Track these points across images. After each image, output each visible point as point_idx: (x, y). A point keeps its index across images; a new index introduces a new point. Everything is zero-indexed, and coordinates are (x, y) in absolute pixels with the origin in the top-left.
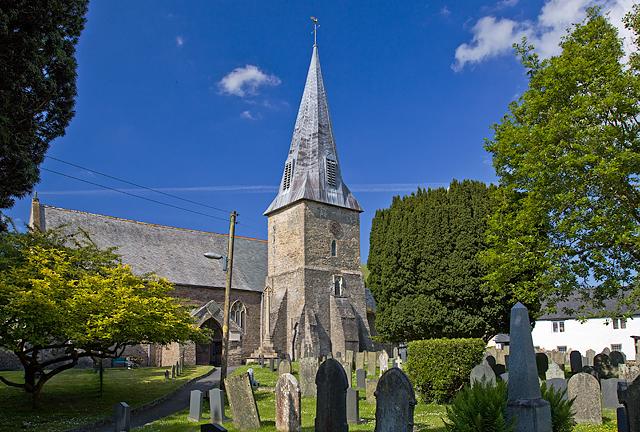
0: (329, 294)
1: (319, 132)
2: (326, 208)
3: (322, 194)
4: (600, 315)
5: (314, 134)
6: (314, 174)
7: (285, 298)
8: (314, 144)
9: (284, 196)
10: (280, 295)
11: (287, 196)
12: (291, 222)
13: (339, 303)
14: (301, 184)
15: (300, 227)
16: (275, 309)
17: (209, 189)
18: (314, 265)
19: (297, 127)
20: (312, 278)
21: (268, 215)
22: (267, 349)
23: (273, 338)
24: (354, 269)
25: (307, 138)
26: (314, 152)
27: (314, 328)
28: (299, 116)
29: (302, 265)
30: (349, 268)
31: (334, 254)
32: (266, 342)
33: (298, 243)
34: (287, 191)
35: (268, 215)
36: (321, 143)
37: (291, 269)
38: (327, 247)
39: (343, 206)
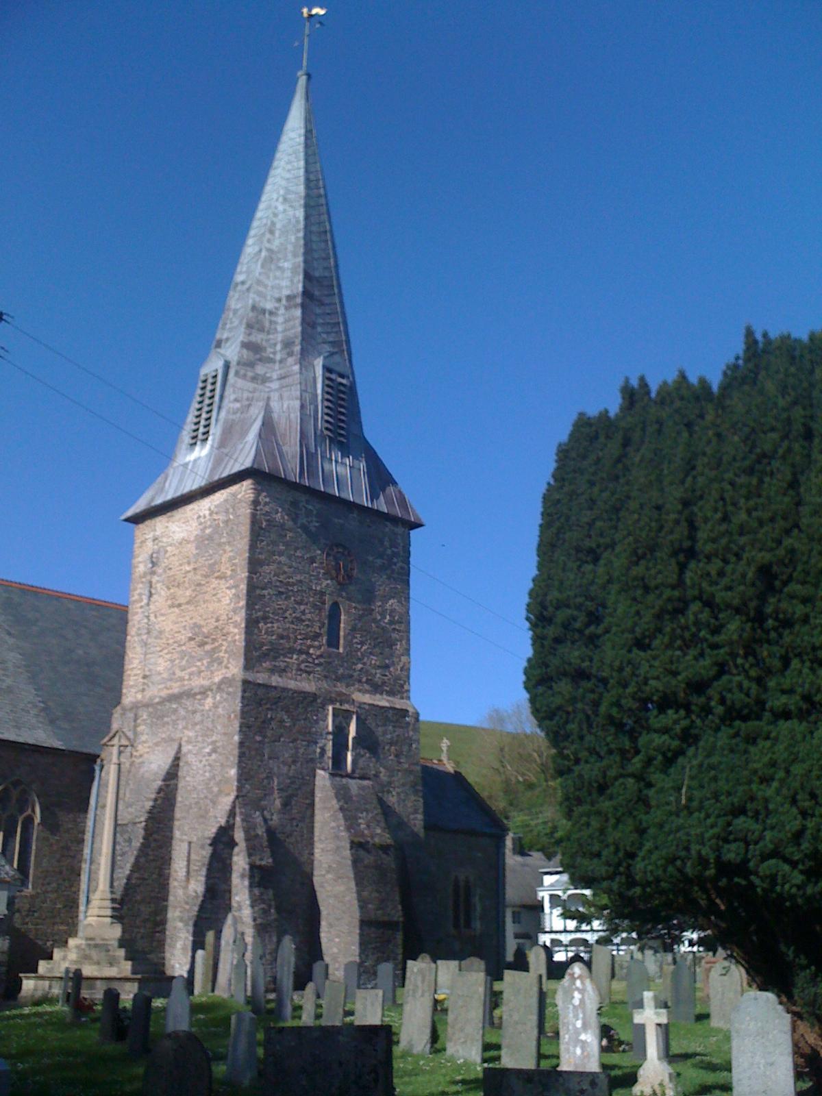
0: (311, 764)
1: (306, 293)
2: (315, 506)
3: (308, 460)
4: (312, 177)
5: (289, 298)
6: (287, 407)
7: (172, 775)
8: (288, 323)
9: (195, 461)
10: (155, 762)
11: (202, 463)
12: (205, 541)
13: (342, 795)
14: (244, 433)
15: (234, 555)
16: (138, 810)
17: (305, 56)
18: (272, 671)
19: (239, 278)
20: (267, 716)
21: (137, 519)
22: (96, 945)
23: (122, 908)
24: (391, 693)
25: (269, 306)
26: (287, 344)
27: (260, 877)
28: (251, 247)
29: (235, 669)
30: (377, 689)
31: (333, 641)
32: (96, 915)
33: (226, 602)
34: (202, 452)
35: (137, 519)
36: (308, 323)
37: (198, 683)
38: (316, 621)
39: (366, 503)
